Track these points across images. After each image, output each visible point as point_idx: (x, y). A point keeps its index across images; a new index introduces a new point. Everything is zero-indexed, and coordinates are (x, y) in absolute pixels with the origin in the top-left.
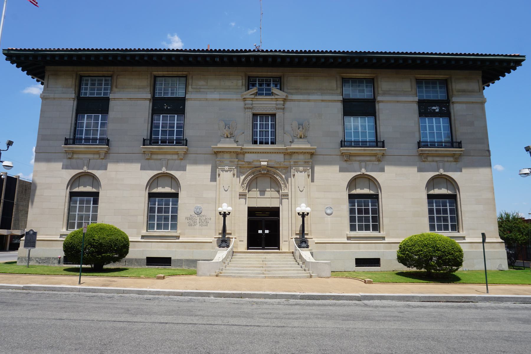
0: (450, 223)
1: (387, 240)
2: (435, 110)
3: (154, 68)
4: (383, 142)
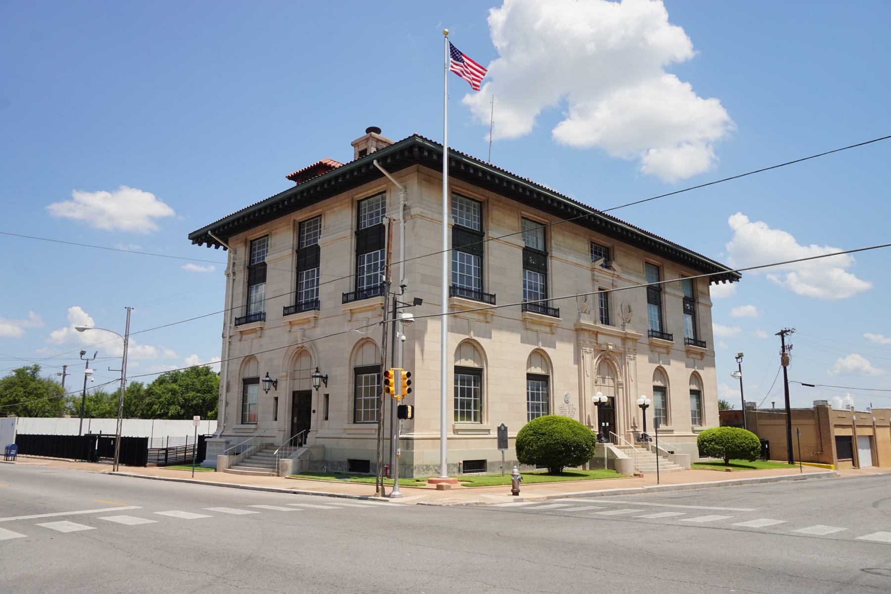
0: (473, 410)
1: (675, 433)
3: (524, 206)
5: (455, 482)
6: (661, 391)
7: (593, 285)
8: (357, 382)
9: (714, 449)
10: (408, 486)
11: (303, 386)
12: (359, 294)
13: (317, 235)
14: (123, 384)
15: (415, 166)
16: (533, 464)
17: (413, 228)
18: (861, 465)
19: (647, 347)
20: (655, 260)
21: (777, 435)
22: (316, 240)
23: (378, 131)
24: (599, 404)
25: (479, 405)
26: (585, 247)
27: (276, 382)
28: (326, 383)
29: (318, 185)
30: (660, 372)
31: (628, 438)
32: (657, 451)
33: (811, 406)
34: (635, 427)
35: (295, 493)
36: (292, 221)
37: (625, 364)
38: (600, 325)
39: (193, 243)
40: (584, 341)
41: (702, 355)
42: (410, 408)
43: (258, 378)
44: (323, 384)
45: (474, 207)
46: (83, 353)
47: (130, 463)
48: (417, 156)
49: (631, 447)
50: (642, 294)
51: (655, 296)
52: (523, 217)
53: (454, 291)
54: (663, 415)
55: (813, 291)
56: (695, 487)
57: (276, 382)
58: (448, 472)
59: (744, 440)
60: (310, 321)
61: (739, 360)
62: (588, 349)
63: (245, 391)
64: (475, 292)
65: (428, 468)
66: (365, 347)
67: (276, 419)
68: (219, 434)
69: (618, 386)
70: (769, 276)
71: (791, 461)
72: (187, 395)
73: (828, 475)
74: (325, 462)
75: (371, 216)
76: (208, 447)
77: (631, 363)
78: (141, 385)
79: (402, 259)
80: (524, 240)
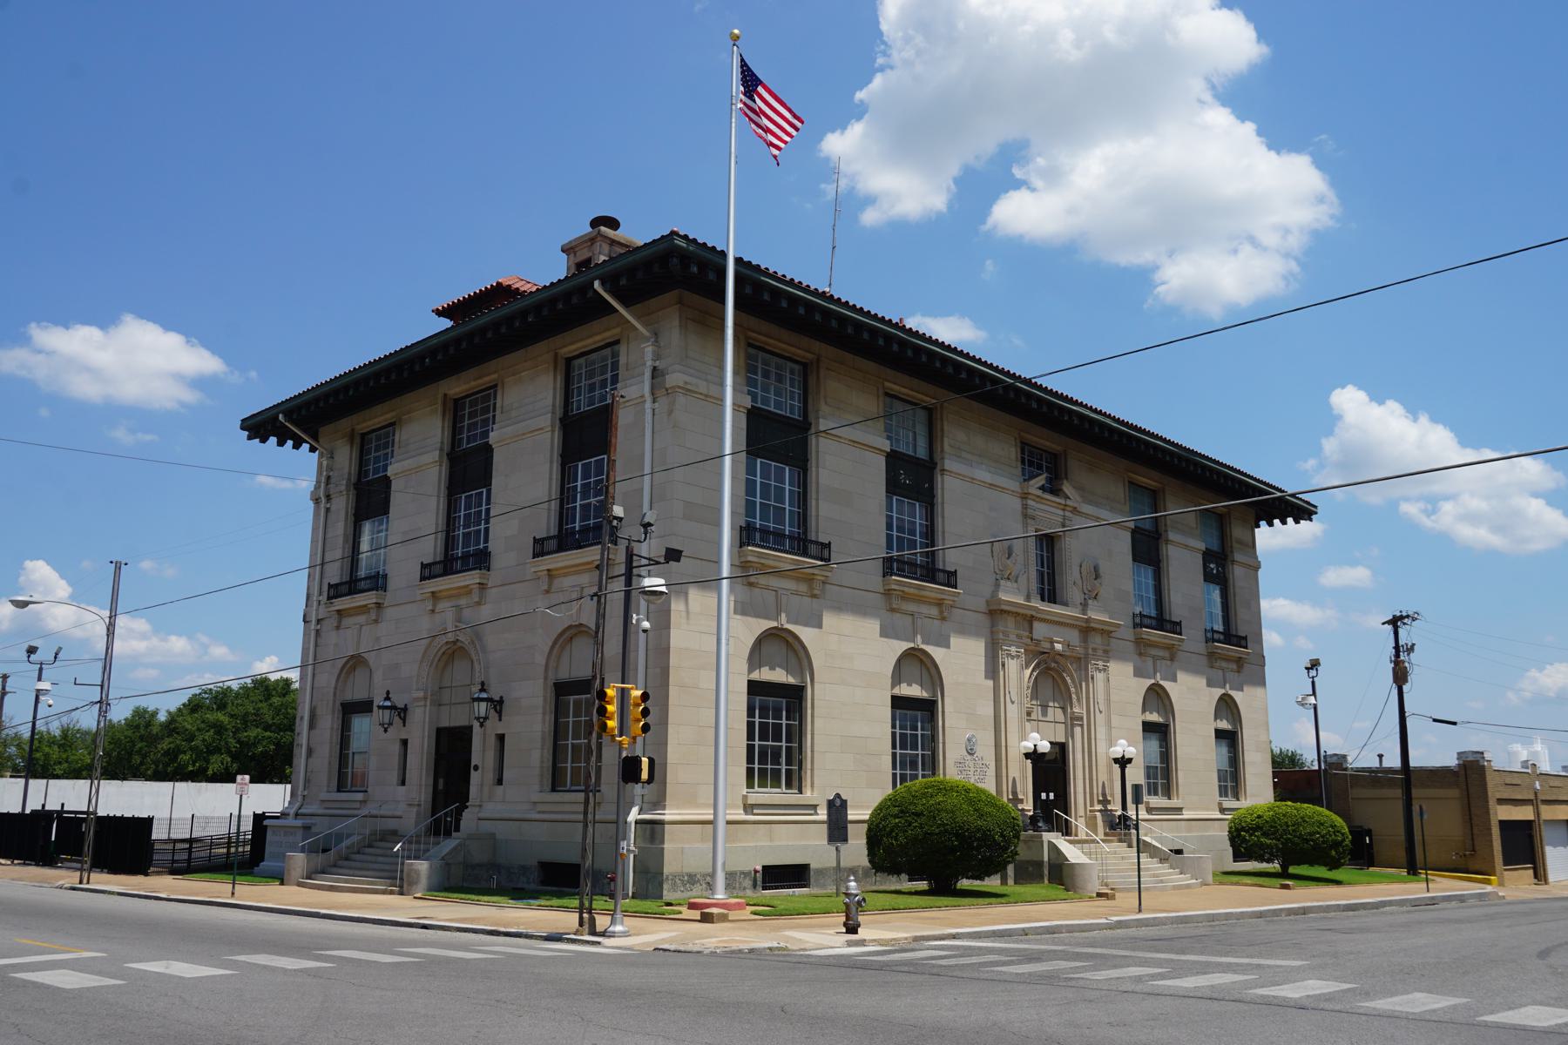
0: (784, 768)
1: (1187, 815)
5: (739, 906)
6: (1159, 732)
7: (1025, 526)
8: (559, 711)
9: (1262, 846)
10: (646, 914)
11: (456, 719)
12: (565, 540)
13: (487, 424)
14: (103, 713)
15: (676, 292)
16: (899, 874)
17: (670, 412)
18: (1551, 878)
19: (1130, 646)
20: (1148, 479)
21: (1385, 819)
22: (486, 434)
23: (613, 223)
24: (1034, 756)
25: (796, 757)
26: (1011, 452)
27: (405, 709)
28: (500, 713)
29: (491, 327)
30: (1157, 697)
31: (1091, 824)
32: (1142, 847)
33: (1451, 761)
34: (1105, 802)
35: (425, 927)
36: (440, 396)
37: (1088, 679)
38: (1037, 603)
39: (249, 438)
40: (1006, 634)
41: (1240, 662)
42: (645, 760)
43: (371, 702)
44: (493, 713)
45: (792, 372)
46: (32, 650)
47: (115, 869)
48: (676, 274)
49: (1094, 841)
50: (1123, 544)
51: (1147, 548)
52: (887, 394)
53: (747, 535)
54: (1162, 776)
55: (1478, 535)
56: (1212, 918)
57: (405, 709)
58: (728, 887)
59: (1326, 824)
60: (470, 592)
61: (1313, 673)
62: (1013, 649)
63: (345, 727)
64: (791, 537)
65: (692, 879)
66: (575, 642)
67: (403, 783)
68: (292, 812)
69: (1073, 721)
70: (1406, 508)
71: (1413, 870)
72: (228, 734)
73: (1481, 896)
74: (494, 867)
75: (592, 388)
76: (269, 836)
77: (1099, 677)
78: (155, 713)
79: (647, 470)
80: (889, 438)
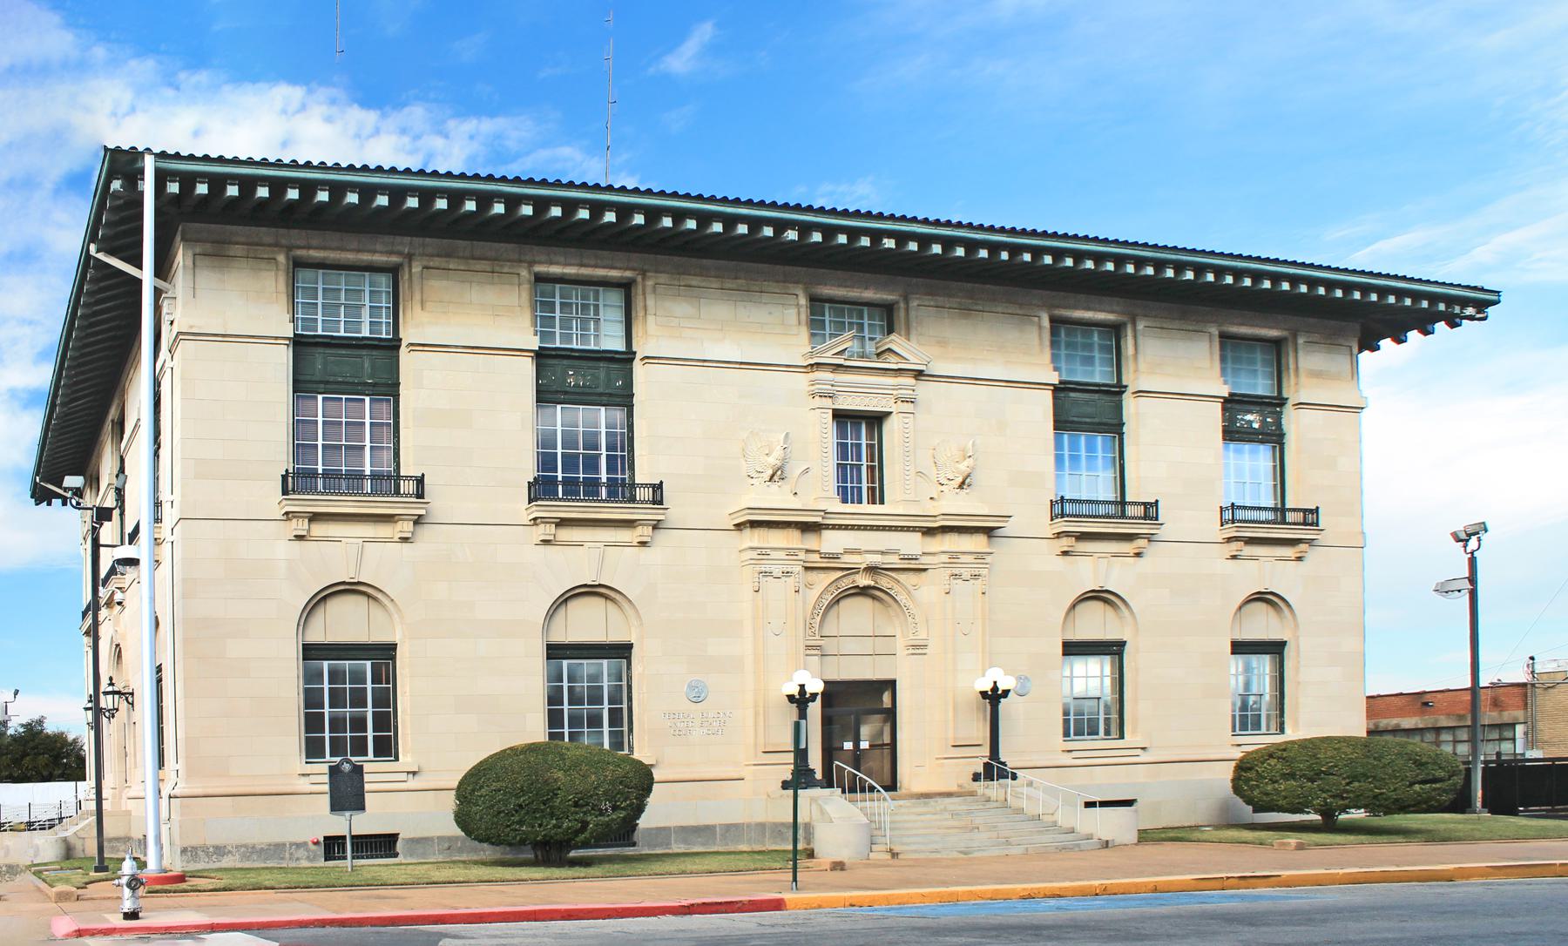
2: (1250, 422)
4: (420, 481)
